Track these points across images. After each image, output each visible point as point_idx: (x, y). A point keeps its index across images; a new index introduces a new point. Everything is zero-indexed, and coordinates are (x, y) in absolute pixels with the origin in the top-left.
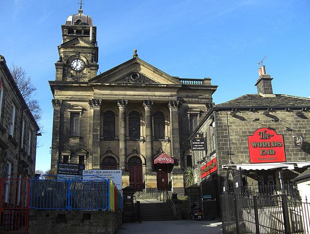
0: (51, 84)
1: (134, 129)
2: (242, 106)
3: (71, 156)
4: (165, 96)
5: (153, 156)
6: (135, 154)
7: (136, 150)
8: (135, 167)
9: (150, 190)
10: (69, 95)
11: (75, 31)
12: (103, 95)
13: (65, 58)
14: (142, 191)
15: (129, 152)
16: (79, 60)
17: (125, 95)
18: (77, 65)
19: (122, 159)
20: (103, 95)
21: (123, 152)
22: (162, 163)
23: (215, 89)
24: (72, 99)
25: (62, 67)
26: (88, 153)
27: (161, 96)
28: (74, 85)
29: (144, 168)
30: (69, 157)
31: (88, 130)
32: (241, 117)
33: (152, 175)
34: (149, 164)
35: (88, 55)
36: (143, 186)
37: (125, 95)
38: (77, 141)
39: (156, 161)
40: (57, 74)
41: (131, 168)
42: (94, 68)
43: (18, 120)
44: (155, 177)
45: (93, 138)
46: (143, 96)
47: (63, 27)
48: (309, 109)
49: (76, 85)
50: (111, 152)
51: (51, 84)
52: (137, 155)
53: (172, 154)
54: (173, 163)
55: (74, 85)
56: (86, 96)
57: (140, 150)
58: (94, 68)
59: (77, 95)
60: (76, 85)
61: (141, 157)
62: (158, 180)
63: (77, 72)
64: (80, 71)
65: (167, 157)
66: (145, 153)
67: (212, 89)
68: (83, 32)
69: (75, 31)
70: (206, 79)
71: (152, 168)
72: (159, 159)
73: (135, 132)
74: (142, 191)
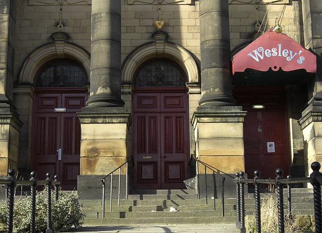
2: (110, 108)
5: (225, 50)
6: (160, 47)
7: (161, 32)
8: (160, 97)
9: (217, 184)
14: (183, 187)
15: (127, 41)
19: (99, 57)
21: (102, 29)
29: (194, 101)
34: (213, 75)
36: (189, 167)
39: (239, 62)
41: (145, 102)
44: (235, 130)
48: (321, 13)
50: (67, 38)
52: (169, 49)
53: (308, 33)
54: (312, 68)
57: (179, 33)
61: (185, 56)
62: (250, 142)
65: (287, 44)
71: (225, 88)
72: (255, 56)
74: (183, 187)
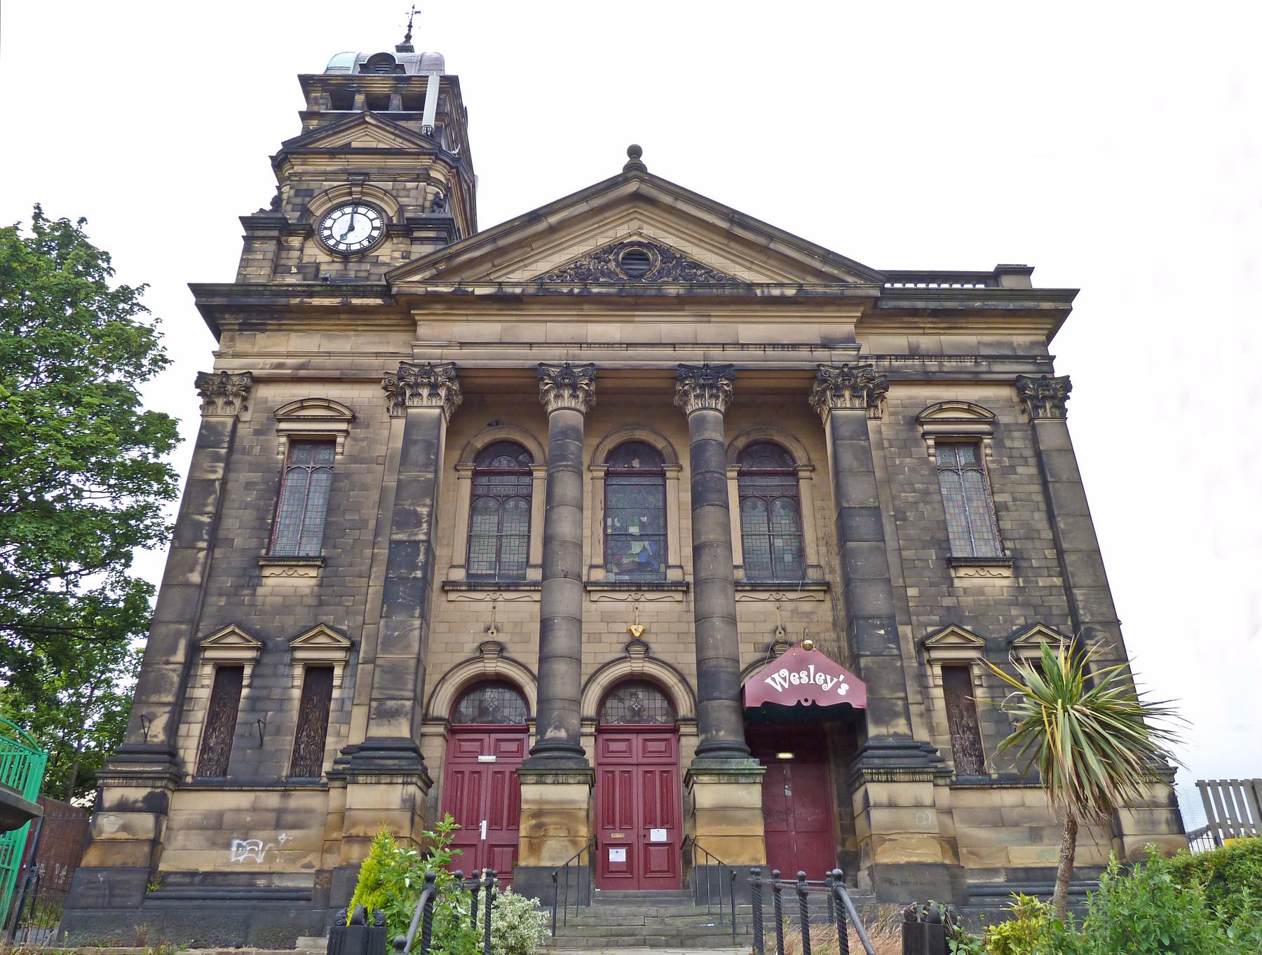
0: (203, 301)
1: (634, 530)
3: (257, 662)
4: (794, 346)
10: (290, 355)
11: (360, 99)
12: (462, 345)
13: (298, 200)
16: (361, 210)
17: (580, 345)
18: (351, 228)
20: (462, 345)
22: (792, 703)
23: (1061, 306)
24: (302, 373)
25: (275, 233)
26: (353, 648)
27: (774, 346)
28: (316, 301)
30: (247, 671)
31: (372, 524)
32: (755, 927)
33: (734, 777)
35: (409, 185)
37: (580, 345)
38: (304, 581)
40: (245, 263)
42: (431, 234)
43: (590, 943)
45: (390, 564)
46: (674, 345)
47: (307, 82)
49: (327, 302)
51: (203, 301)
55: (316, 301)
56: (377, 354)
58: (431, 234)
59: (329, 354)
60: (327, 302)
63: (346, 256)
64: (362, 254)
66: (691, 659)
67: (1046, 305)
68: (396, 101)
69: (360, 99)
70: (1003, 271)
73: (636, 547)
